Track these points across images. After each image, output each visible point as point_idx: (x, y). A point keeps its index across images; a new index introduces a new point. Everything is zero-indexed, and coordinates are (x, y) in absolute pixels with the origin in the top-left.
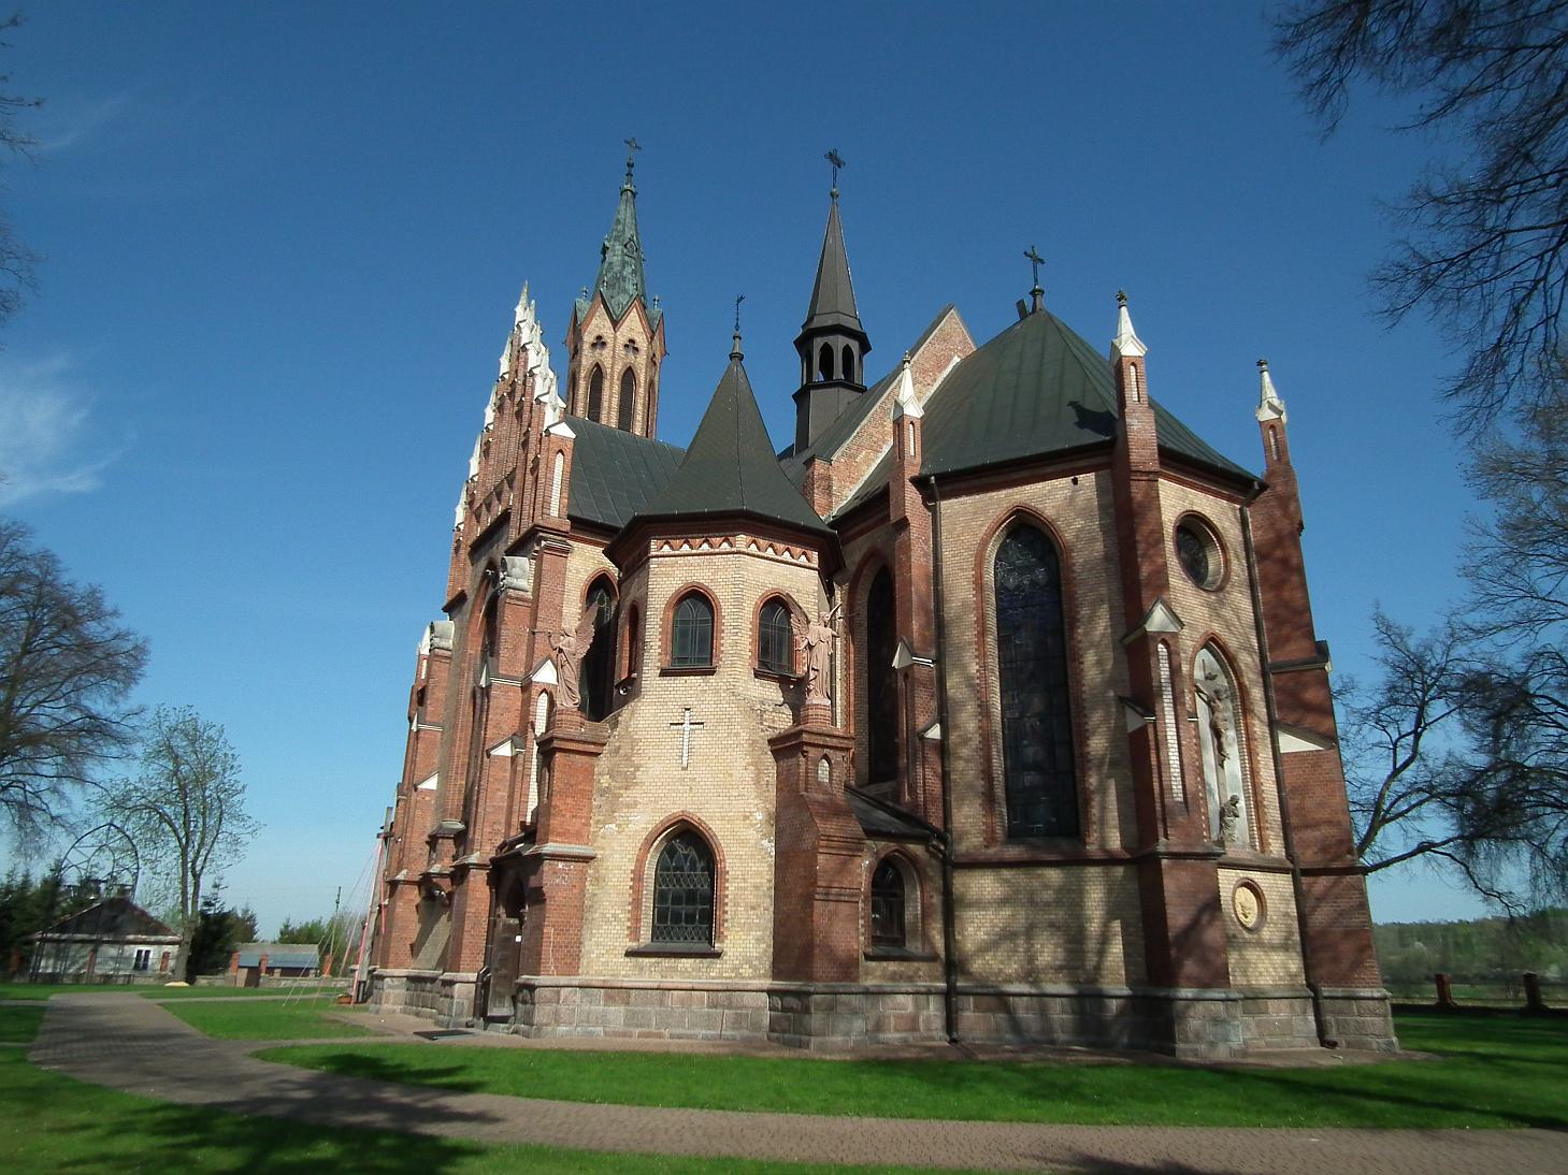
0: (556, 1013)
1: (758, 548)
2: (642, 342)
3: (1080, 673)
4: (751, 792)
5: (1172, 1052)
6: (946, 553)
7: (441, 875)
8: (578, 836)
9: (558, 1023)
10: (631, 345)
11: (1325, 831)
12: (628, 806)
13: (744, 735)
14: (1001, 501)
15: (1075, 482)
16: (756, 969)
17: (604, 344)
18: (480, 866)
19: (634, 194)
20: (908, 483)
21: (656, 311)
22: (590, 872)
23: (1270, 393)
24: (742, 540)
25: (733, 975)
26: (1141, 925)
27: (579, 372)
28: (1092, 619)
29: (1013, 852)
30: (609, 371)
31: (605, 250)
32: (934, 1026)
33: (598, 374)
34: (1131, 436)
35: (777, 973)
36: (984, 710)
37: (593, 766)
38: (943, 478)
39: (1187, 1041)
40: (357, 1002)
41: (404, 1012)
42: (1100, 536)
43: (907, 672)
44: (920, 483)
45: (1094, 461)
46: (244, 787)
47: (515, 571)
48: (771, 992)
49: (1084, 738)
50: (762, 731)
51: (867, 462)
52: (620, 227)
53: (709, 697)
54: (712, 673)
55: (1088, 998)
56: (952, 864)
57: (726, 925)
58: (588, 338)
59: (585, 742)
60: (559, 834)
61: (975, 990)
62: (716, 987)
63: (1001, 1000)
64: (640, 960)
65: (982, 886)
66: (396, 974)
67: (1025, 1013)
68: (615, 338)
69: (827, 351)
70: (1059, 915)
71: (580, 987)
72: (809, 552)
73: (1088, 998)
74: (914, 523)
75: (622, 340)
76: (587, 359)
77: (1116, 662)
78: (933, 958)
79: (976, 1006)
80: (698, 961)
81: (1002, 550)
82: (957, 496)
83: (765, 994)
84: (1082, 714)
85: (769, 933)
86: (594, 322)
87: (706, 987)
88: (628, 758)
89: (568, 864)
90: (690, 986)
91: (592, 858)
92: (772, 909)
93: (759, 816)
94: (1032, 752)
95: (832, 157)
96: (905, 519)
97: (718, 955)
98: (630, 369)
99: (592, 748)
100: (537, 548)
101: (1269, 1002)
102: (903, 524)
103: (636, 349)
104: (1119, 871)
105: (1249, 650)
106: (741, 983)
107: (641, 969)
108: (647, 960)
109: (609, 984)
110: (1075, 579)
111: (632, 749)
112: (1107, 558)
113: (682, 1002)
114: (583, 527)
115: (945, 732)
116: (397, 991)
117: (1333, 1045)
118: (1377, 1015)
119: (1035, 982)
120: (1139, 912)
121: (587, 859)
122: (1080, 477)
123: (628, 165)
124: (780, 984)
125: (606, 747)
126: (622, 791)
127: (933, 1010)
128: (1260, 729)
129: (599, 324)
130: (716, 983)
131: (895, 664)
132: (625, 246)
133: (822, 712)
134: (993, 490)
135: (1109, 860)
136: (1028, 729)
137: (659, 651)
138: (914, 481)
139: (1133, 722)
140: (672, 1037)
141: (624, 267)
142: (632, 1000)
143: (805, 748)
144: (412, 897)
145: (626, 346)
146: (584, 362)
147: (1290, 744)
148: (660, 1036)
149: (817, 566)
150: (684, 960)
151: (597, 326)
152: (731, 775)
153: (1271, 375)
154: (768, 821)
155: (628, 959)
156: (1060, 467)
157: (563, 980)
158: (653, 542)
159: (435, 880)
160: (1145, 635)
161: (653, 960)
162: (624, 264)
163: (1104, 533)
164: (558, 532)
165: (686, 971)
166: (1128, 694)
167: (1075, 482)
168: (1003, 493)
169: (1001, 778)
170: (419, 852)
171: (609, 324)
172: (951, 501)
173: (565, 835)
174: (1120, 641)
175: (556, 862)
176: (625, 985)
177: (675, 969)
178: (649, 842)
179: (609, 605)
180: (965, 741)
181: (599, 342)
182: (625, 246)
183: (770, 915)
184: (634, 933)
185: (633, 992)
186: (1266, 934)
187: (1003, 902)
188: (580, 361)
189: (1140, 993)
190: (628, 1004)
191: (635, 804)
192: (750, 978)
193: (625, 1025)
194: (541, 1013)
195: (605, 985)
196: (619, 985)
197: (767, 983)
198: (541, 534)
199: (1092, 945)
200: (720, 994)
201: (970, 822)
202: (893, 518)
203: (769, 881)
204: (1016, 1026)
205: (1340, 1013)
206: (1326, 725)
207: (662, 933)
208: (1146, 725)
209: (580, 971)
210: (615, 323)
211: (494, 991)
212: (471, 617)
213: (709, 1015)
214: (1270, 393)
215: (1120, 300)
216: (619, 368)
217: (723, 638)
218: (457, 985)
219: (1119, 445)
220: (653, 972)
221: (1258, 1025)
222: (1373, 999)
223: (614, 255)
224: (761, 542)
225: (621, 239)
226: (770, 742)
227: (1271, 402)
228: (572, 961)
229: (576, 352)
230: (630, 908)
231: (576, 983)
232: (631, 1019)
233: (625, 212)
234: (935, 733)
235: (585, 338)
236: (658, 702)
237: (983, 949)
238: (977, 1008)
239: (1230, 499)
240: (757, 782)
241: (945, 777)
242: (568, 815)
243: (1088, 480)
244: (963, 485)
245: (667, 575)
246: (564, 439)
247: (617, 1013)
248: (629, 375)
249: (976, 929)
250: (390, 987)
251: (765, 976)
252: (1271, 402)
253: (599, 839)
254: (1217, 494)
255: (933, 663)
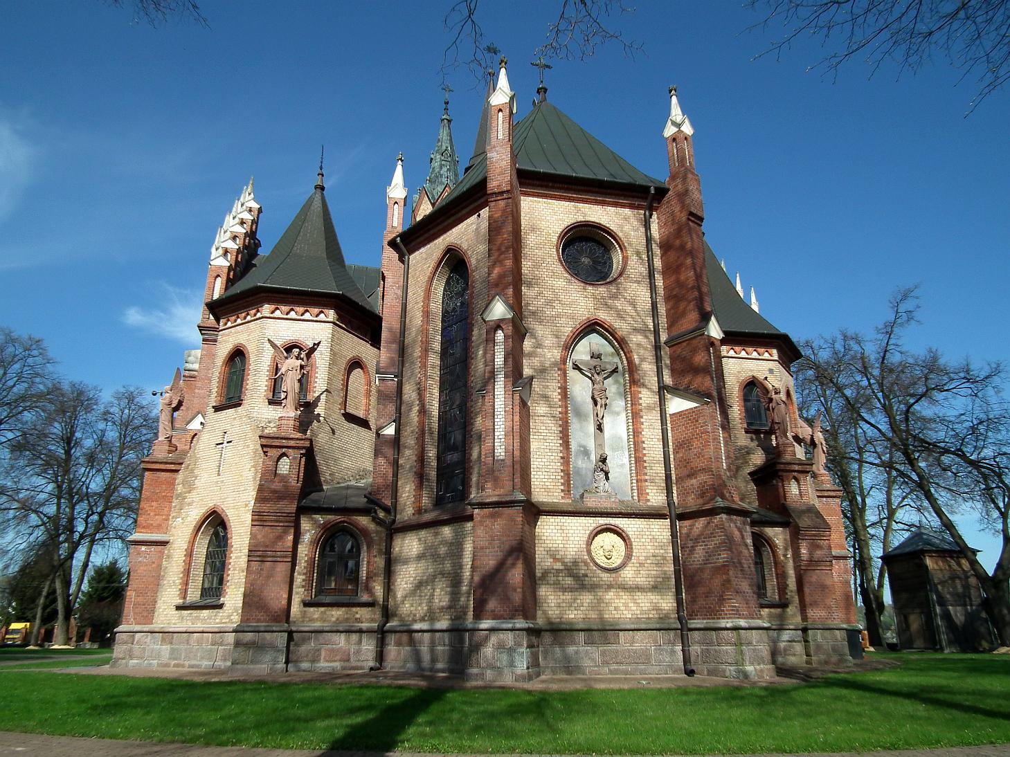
0: (131, 650)
1: (759, 354)
8: (159, 528)
9: (131, 657)
11: (703, 477)
13: (252, 447)
19: (449, 121)
22: (166, 552)
23: (676, 112)
25: (228, 620)
32: (440, 666)
36: (423, 411)
37: (175, 479)
39: (478, 666)
53: (237, 422)
54: (240, 405)
56: (394, 530)
59: (166, 463)
60: (144, 527)
61: (398, 629)
72: (325, 311)
82: (418, 249)
86: (422, 207)
88: (192, 471)
89: (150, 547)
91: (168, 542)
97: (220, 606)
99: (172, 467)
101: (621, 633)
105: (643, 331)
108: (186, 612)
115: (398, 431)
118: (731, 644)
127: (368, 646)
128: (647, 397)
133: (286, 422)
141: (441, 168)
142: (174, 641)
147: (677, 405)
150: (204, 611)
151: (424, 209)
155: (177, 612)
157: (138, 628)
162: (441, 167)
169: (434, 464)
173: (148, 528)
175: (140, 547)
177: (197, 618)
184: (184, 594)
186: (628, 574)
187: (420, 557)
191: (193, 502)
206: (707, 383)
213: (211, 650)
221: (603, 654)
224: (737, 348)
227: (678, 120)
228: (149, 612)
231: (147, 629)
239: (631, 207)
242: (152, 514)
246: (220, 267)
252: (678, 120)
254: (603, 203)
255: (395, 377)
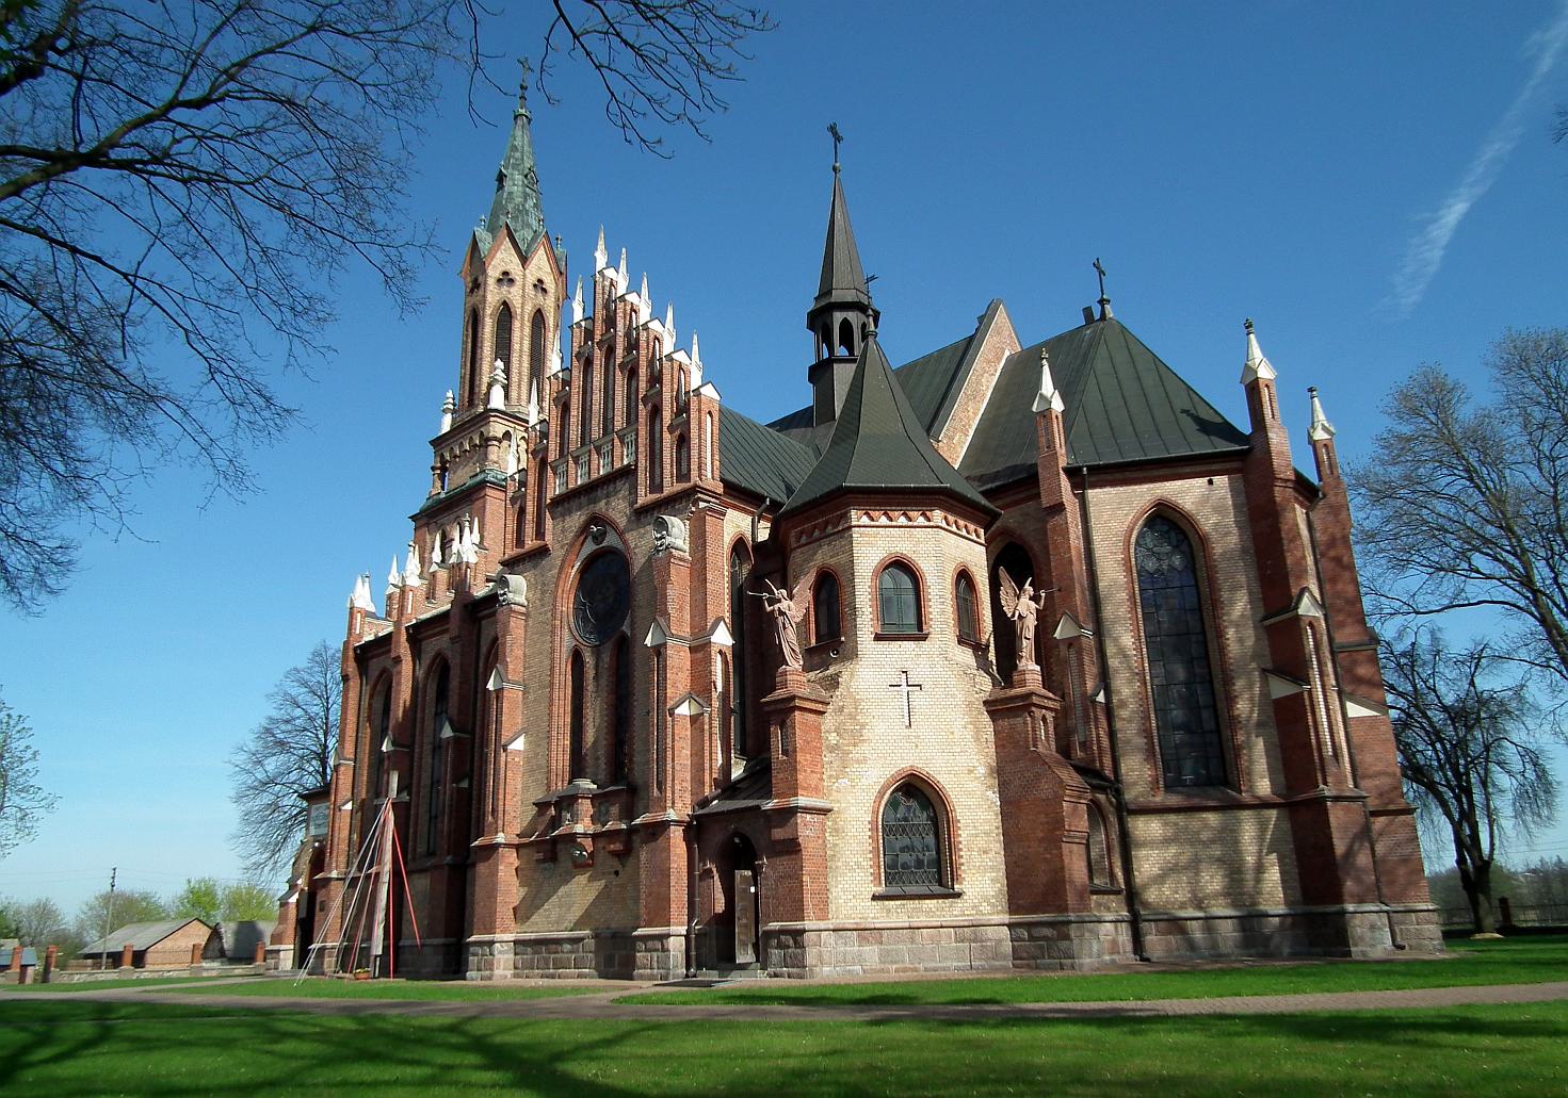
2: (550, 284)
3: (1222, 649)
4: (972, 747)
5: (1349, 954)
6: (1096, 537)
7: (585, 835)
10: (539, 285)
12: (858, 762)
13: (960, 697)
14: (1143, 495)
15: (1210, 482)
16: (992, 905)
17: (511, 281)
18: (678, 823)
19: (530, 121)
20: (1061, 471)
21: (560, 250)
23: (1320, 416)
24: (938, 516)
26: (1294, 857)
27: (484, 309)
28: (1232, 603)
29: (1174, 800)
30: (519, 311)
31: (501, 178)
33: (506, 314)
34: (1273, 448)
35: (1014, 906)
38: (1093, 469)
40: (374, 978)
41: (515, 976)
42: (1235, 531)
43: (1071, 643)
44: (1071, 472)
45: (1228, 466)
46: (35, 753)
47: (675, 531)
48: (1010, 926)
49: (1231, 700)
50: (977, 693)
51: (961, 443)
52: (518, 155)
55: (1250, 920)
56: (1124, 810)
57: (963, 868)
58: (493, 273)
60: (804, 789)
62: (962, 924)
63: (1175, 925)
64: (887, 903)
65: (1147, 828)
66: (506, 939)
67: (1196, 931)
68: (524, 275)
69: (846, 326)
70: (1217, 851)
71: (833, 930)
73: (1250, 920)
74: (1069, 507)
75: (531, 280)
76: (493, 295)
77: (1258, 639)
78: (1118, 893)
79: (1157, 931)
80: (940, 901)
81: (1141, 535)
82: (1101, 486)
83: (1006, 928)
84: (1228, 681)
85: (1002, 873)
86: (499, 255)
87: (954, 924)
88: (852, 717)
90: (939, 924)
91: (830, 811)
92: (1003, 853)
93: (982, 770)
94: (1177, 714)
95: (832, 129)
96: (1062, 504)
97: (958, 895)
98: (539, 311)
99: (820, 707)
100: (693, 509)
102: (1059, 508)
103: (544, 290)
104: (1273, 813)
106: (984, 919)
107: (889, 911)
108: (892, 903)
109: (862, 927)
110: (1216, 566)
111: (856, 709)
112: (1244, 550)
113: (932, 938)
114: (739, 494)
115: (1108, 696)
116: (507, 956)
117: (1402, 948)
118: (1432, 924)
119: (1200, 908)
120: (1292, 846)
121: (825, 812)
122: (1215, 479)
123: (522, 87)
124: (1017, 918)
125: (830, 706)
126: (851, 748)
129: (503, 259)
130: (961, 920)
131: (1057, 635)
132: (526, 176)
134: (1136, 484)
135: (1265, 805)
136: (1176, 695)
137: (871, 616)
138: (1064, 469)
139: (1281, 689)
140: (926, 970)
141: (526, 200)
143: (1033, 709)
144: (511, 860)
145: (535, 286)
146: (489, 298)
148: (916, 970)
149: (984, 542)
150: (927, 901)
152: (952, 733)
153: (1320, 401)
154: (990, 775)
155: (874, 903)
156: (1198, 469)
158: (853, 512)
159: (579, 840)
160: (1298, 618)
161: (898, 902)
163: (1240, 528)
164: (714, 495)
165: (931, 911)
166: (1269, 666)
167: (1210, 482)
168: (1145, 487)
170: (513, 814)
171: (516, 260)
172: (1096, 490)
174: (1262, 621)
176: (878, 926)
178: (881, 794)
179: (740, 568)
180: (1123, 704)
181: (506, 279)
182: (526, 176)
183: (1001, 858)
185: (885, 933)
187: (1166, 842)
188: (484, 296)
189: (1299, 911)
190: (881, 943)
191: (865, 760)
192: (991, 914)
193: (881, 962)
194: (811, 955)
195: (859, 927)
196: (872, 926)
197: (1006, 918)
198: (699, 495)
199: (1249, 876)
200: (966, 929)
201: (1137, 773)
202: (1045, 502)
203: (997, 828)
204: (1192, 945)
205: (1403, 923)
207: (894, 879)
208: (1302, 693)
209: (830, 916)
210: (524, 260)
211: (739, 940)
212: (560, 573)
214: (1320, 416)
215: (1247, 328)
216: (529, 309)
217: (930, 607)
218: (672, 938)
219: (1258, 454)
220: (899, 913)
222: (1428, 911)
223: (515, 185)
225: (520, 168)
226: (985, 703)
229: (476, 285)
230: (871, 856)
232: (885, 957)
233: (521, 138)
234: (1101, 698)
235: (490, 272)
236: (873, 666)
237: (1160, 879)
238: (1159, 932)
240: (977, 739)
241: (1112, 734)
243: (1221, 481)
244: (1109, 477)
245: (871, 544)
246: (711, 400)
247: (871, 952)
248: (538, 318)
249: (1148, 864)
250: (500, 952)
251: (1002, 912)
253: (834, 793)
